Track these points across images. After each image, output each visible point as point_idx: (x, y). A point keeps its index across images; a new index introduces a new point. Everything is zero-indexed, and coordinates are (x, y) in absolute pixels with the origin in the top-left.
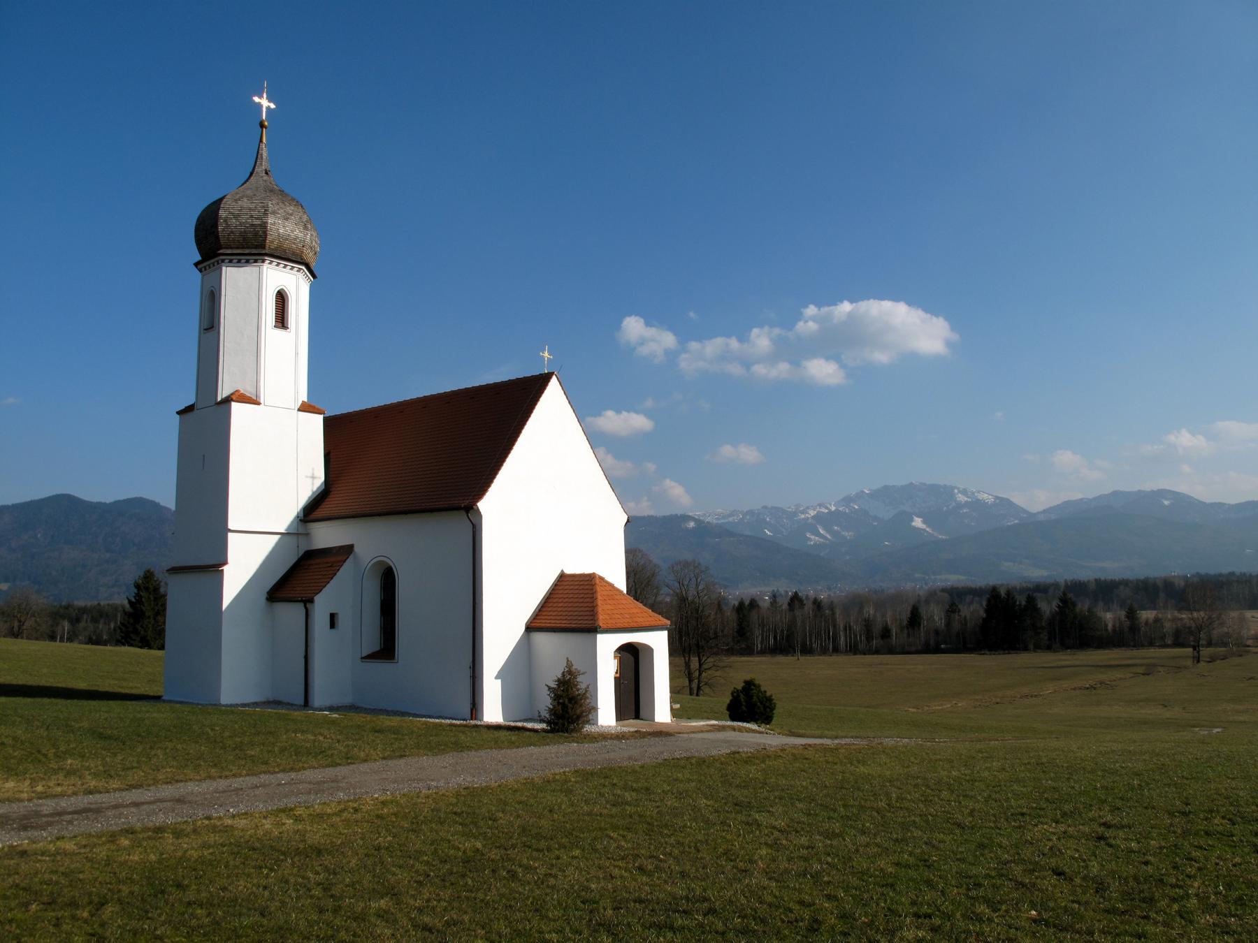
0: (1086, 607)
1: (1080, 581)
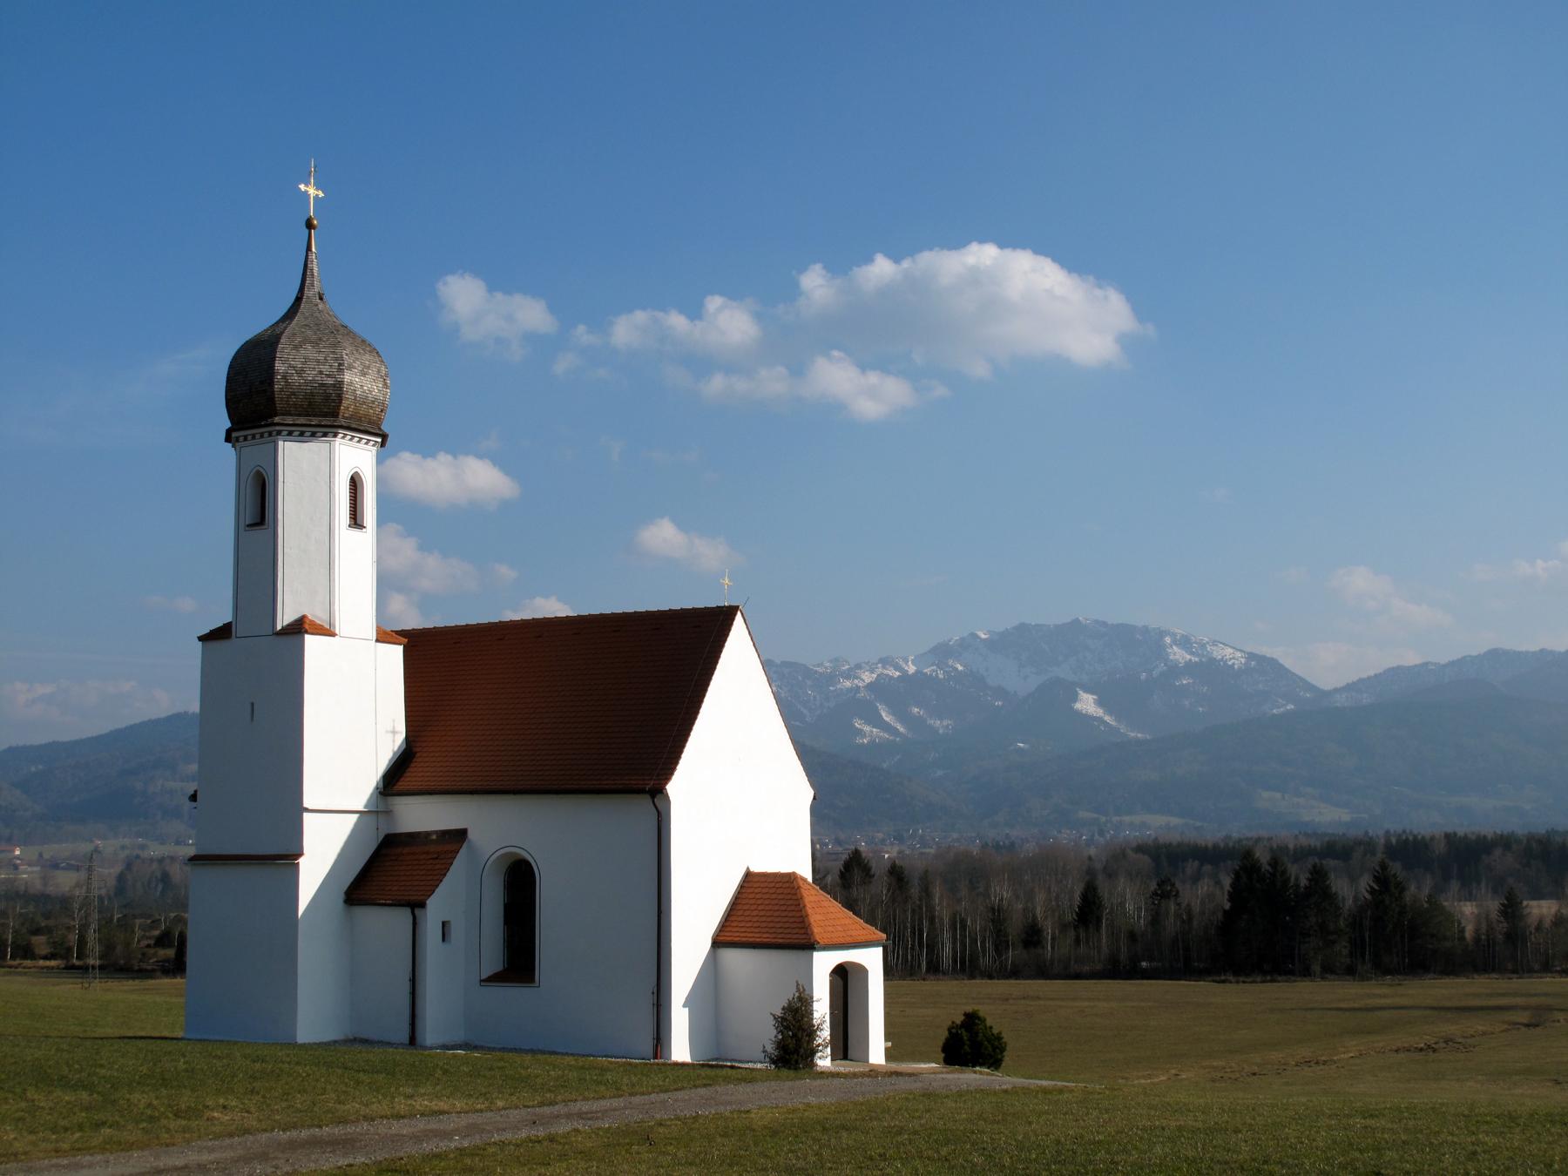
0: (1426, 891)
1: (1415, 837)
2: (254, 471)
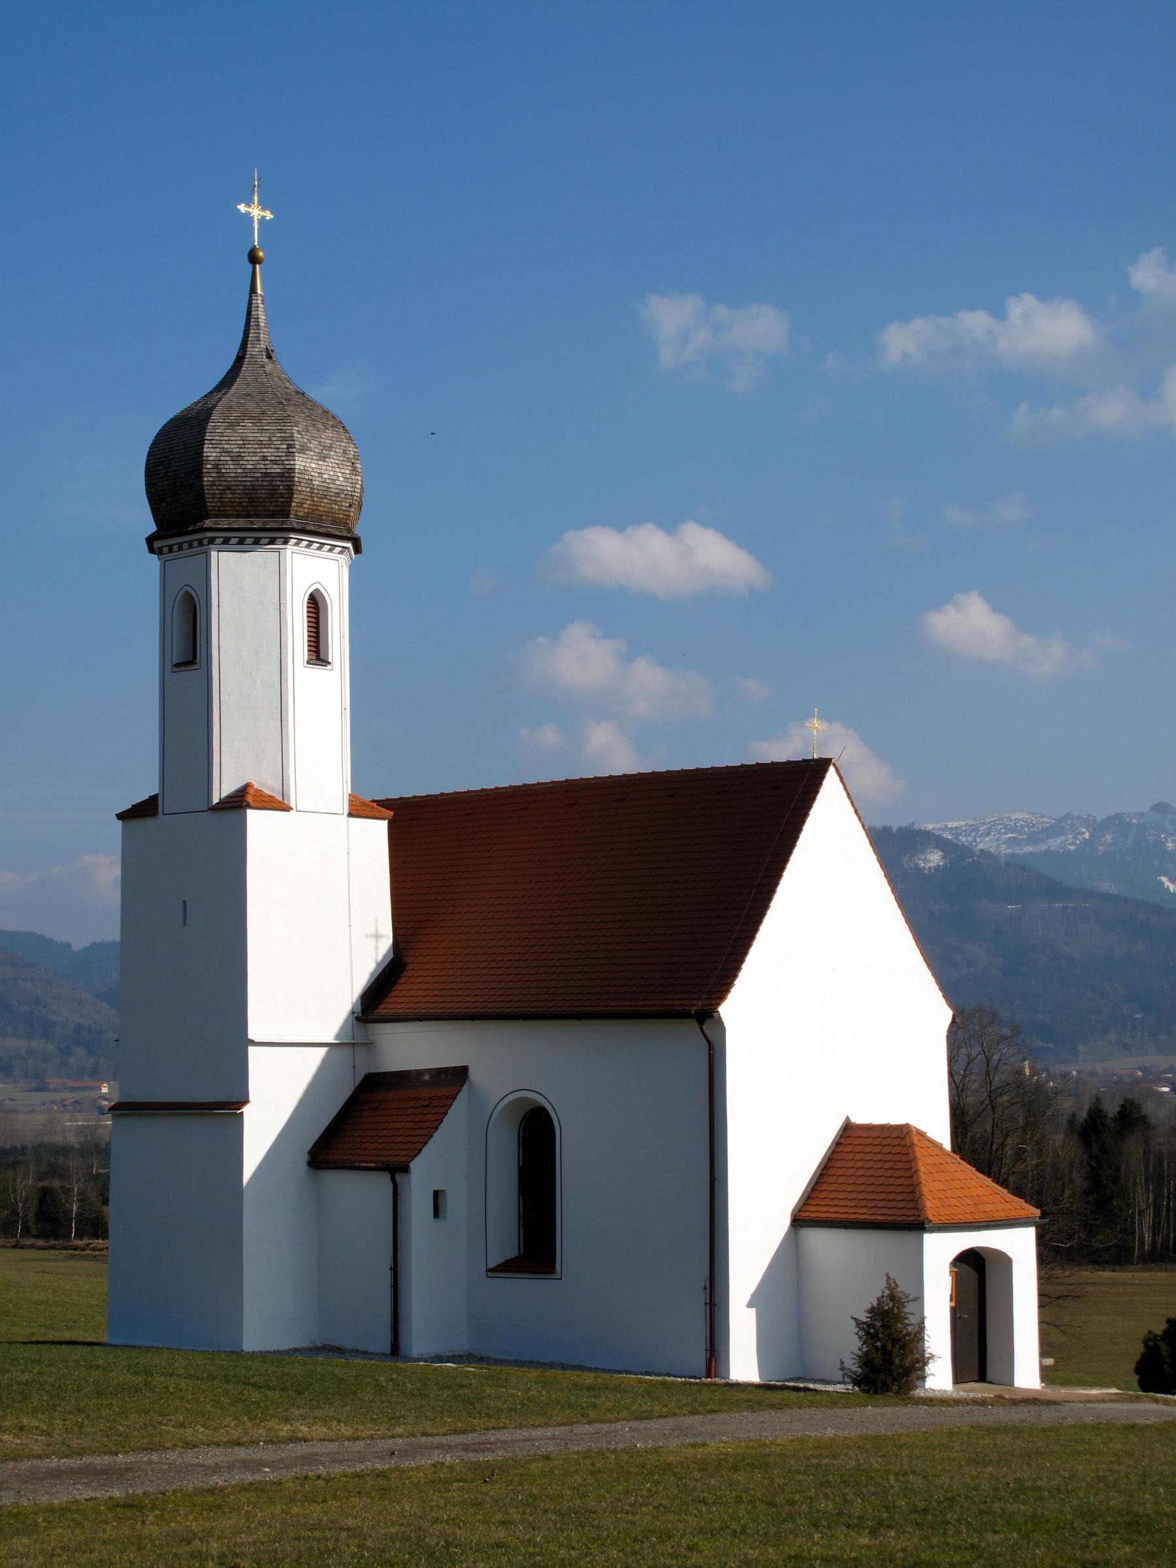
2: (182, 592)
